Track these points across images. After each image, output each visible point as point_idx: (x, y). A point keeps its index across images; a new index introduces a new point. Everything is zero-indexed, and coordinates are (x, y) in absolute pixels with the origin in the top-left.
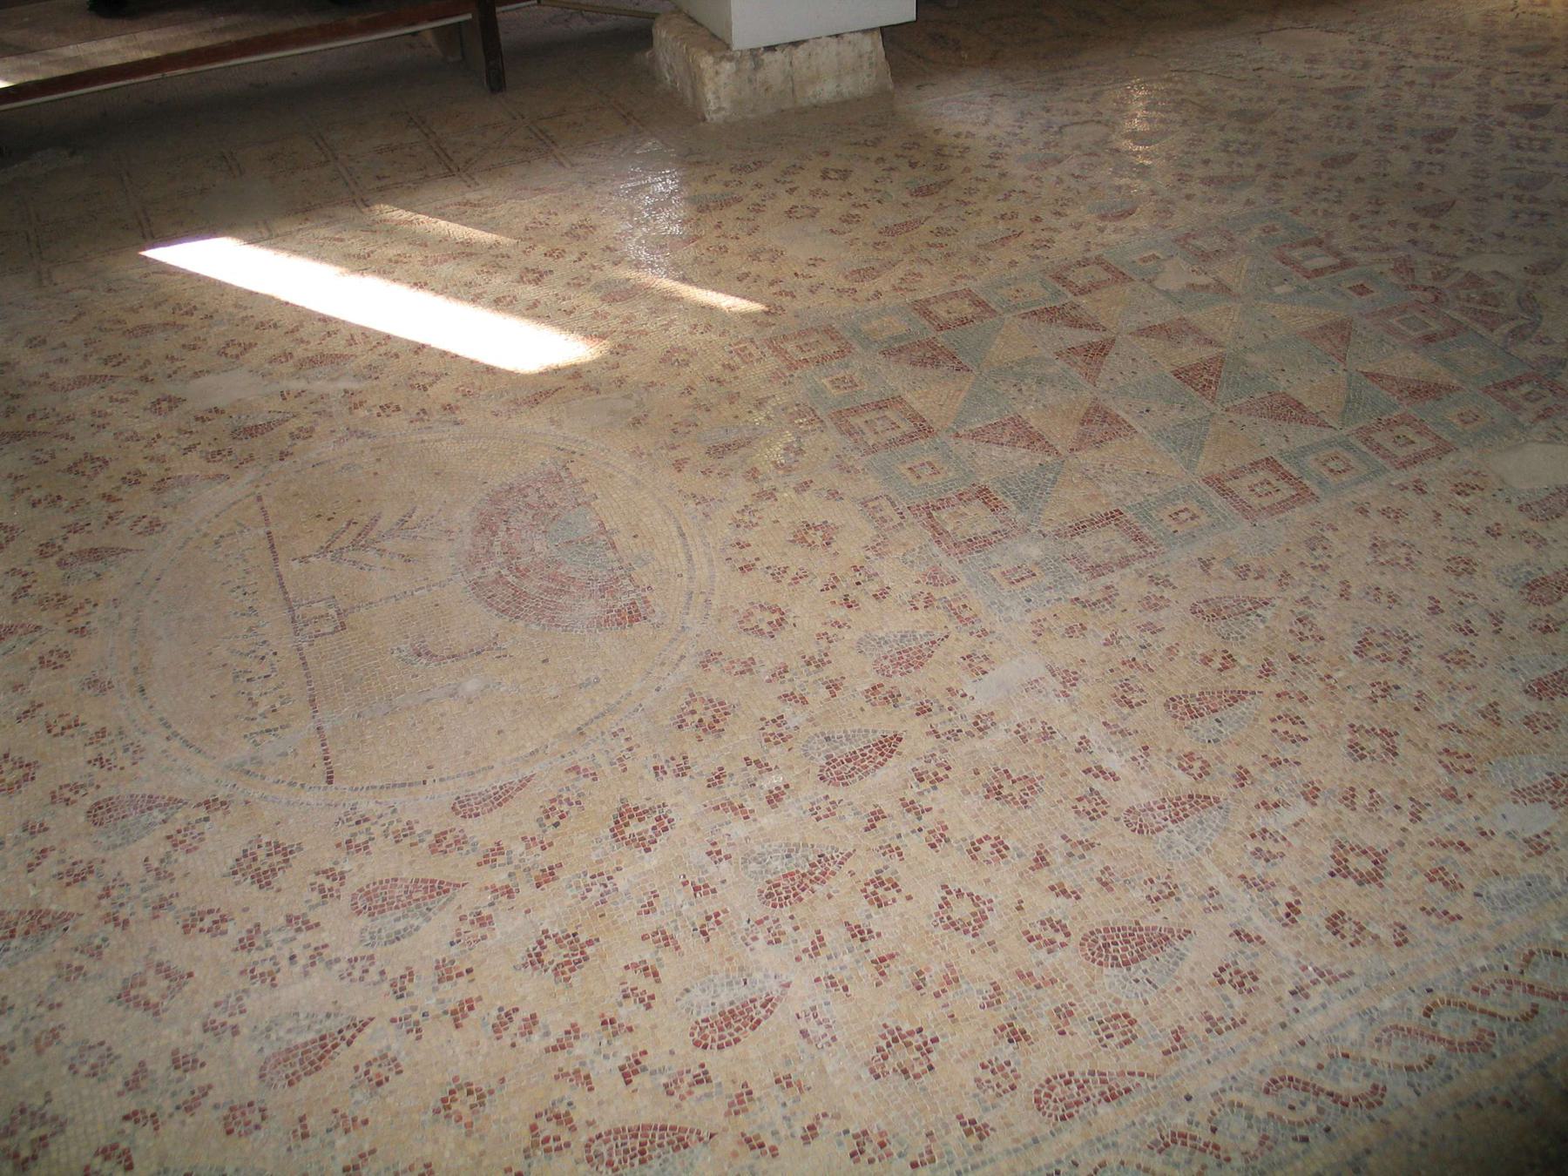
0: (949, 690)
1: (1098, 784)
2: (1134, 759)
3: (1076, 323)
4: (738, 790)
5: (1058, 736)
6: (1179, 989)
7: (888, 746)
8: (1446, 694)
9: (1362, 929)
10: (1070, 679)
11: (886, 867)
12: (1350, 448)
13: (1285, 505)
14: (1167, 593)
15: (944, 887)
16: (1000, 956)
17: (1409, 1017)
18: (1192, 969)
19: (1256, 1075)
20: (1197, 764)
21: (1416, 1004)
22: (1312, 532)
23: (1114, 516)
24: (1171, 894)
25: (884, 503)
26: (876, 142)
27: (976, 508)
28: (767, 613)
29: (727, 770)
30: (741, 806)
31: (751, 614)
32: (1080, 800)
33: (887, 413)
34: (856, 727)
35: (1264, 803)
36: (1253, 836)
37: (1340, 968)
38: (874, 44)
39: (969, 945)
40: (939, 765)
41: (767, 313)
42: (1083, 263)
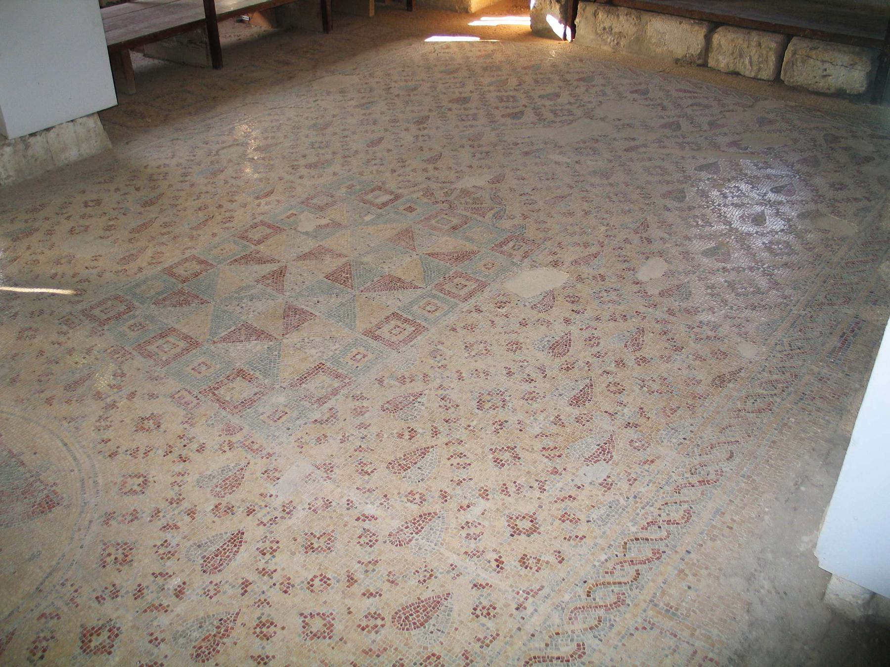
0: (261, 495)
1: (367, 525)
2: (382, 504)
3: (261, 261)
4: (155, 595)
5: (334, 504)
6: (456, 629)
7: (237, 539)
8: (532, 418)
9: (539, 560)
10: (329, 468)
11: (263, 614)
12: (434, 297)
13: (411, 337)
14: (365, 403)
15: (302, 614)
16: (349, 644)
17: (581, 600)
18: (459, 615)
19: (516, 662)
20: (417, 496)
21: (581, 591)
22: (432, 347)
23: (320, 367)
24: (431, 576)
25: (184, 393)
26: (111, 179)
27: (239, 383)
28: (135, 479)
29: (144, 585)
30: (160, 605)
31: (126, 483)
32: (360, 537)
33: (169, 339)
34: (214, 534)
35: (461, 507)
36: (463, 528)
37: (536, 587)
38: (95, 122)
39: (329, 645)
40: (272, 542)
41: (76, 295)
42: (255, 226)
